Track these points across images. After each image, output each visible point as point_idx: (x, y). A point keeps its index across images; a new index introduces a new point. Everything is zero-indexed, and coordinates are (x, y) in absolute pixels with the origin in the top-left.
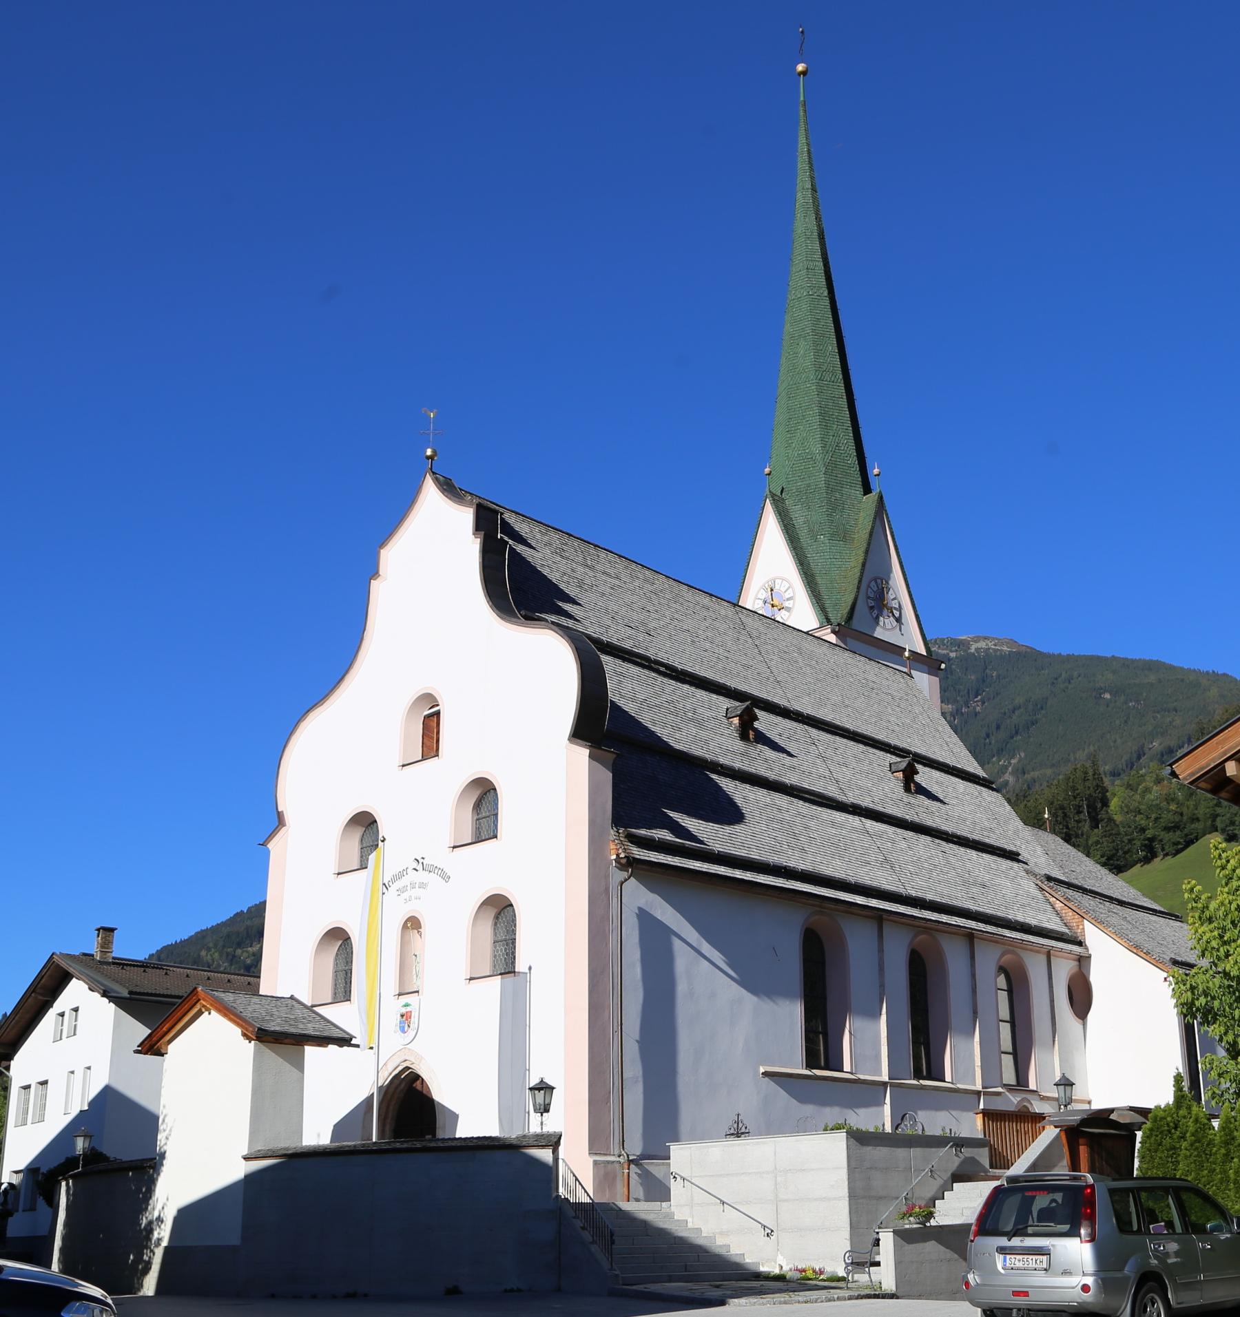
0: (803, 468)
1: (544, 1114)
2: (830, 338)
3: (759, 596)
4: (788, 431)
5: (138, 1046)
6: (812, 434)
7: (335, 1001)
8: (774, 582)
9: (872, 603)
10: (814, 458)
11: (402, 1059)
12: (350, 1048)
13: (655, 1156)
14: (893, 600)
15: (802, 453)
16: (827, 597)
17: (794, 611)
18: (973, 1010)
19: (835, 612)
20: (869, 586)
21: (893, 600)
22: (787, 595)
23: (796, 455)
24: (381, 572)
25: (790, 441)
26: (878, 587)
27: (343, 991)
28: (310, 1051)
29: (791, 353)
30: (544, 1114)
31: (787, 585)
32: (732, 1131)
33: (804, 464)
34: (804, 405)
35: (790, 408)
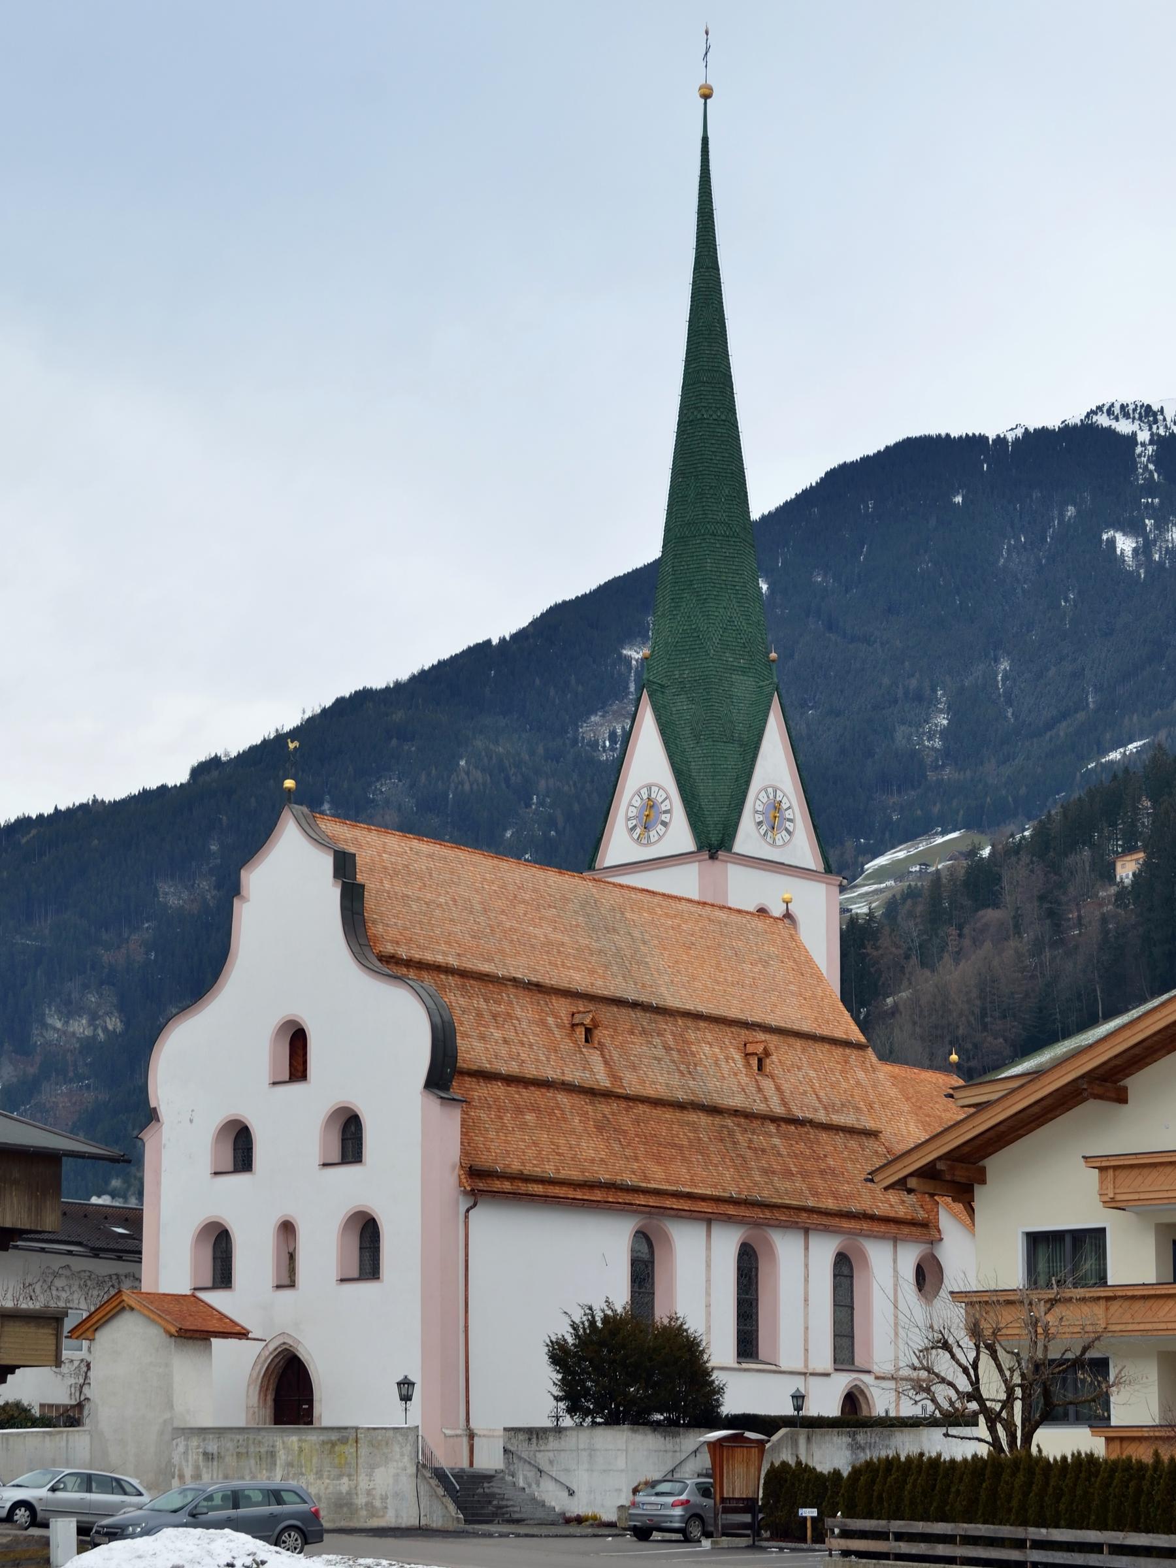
0: (688, 647)
1: (408, 1402)
2: (726, 477)
3: (630, 815)
4: (672, 599)
5: (69, 1333)
6: (700, 606)
7: (214, 1287)
8: (650, 788)
9: (759, 818)
10: (701, 637)
11: (282, 1341)
12: (248, 1341)
13: (924, 1279)
14: (786, 810)
15: (687, 629)
16: (709, 813)
17: (671, 827)
18: (805, 1298)
19: (717, 832)
20: (757, 798)
21: (786, 810)
22: (663, 808)
23: (680, 631)
24: (244, 892)
25: (674, 613)
26: (768, 797)
27: (223, 1277)
28: (215, 1341)
29: (680, 495)
30: (408, 1402)
31: (664, 796)
32: (553, 1414)
33: (689, 643)
34: (692, 566)
35: (675, 569)
